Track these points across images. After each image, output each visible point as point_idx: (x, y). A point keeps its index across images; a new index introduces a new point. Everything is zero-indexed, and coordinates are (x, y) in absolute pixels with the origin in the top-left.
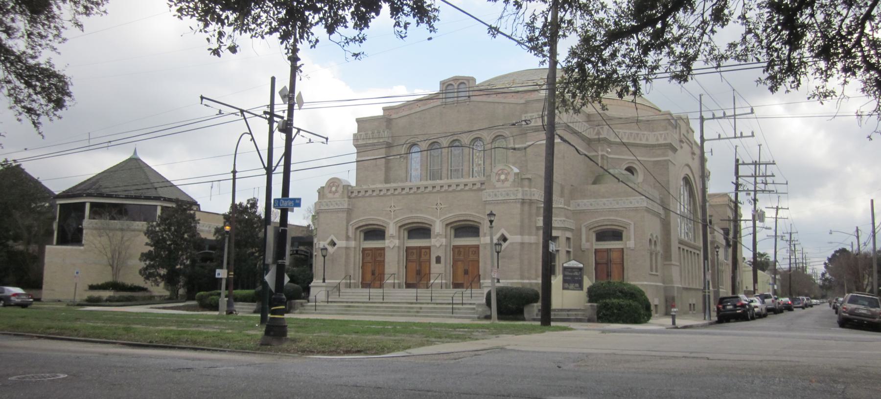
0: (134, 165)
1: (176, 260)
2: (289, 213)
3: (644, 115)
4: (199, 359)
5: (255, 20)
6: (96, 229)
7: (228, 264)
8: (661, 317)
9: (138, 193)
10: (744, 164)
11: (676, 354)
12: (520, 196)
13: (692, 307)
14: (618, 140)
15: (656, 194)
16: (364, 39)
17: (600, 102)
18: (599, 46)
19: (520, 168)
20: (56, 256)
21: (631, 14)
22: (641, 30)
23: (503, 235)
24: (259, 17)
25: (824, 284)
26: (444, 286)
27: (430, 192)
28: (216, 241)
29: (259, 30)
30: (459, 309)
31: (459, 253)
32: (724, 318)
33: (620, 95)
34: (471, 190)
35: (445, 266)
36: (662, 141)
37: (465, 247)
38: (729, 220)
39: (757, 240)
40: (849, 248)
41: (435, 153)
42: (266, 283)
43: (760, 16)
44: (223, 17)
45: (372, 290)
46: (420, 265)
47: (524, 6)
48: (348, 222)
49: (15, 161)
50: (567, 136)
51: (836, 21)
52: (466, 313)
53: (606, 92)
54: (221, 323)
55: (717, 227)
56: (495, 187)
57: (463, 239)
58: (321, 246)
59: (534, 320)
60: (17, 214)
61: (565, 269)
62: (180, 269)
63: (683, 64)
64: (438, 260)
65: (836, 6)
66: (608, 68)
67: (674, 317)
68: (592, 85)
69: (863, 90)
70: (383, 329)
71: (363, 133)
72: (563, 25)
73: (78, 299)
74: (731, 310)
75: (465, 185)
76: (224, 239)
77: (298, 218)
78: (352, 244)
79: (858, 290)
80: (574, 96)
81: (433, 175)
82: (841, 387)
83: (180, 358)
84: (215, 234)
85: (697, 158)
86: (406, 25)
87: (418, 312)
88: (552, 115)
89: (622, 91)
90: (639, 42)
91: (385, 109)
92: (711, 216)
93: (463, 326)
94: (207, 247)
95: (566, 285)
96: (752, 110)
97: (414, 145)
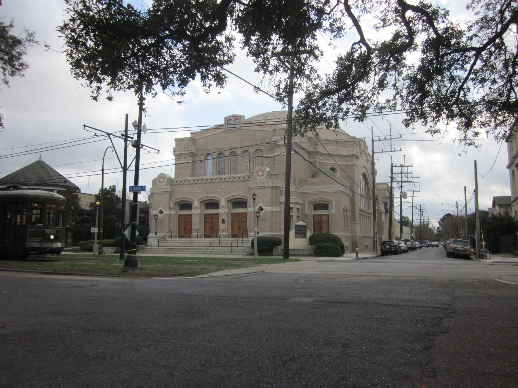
2: (139, 195)
3: (340, 138)
4: (87, 281)
7: (99, 223)
8: (349, 253)
10: (395, 166)
11: (360, 274)
12: (270, 184)
13: (367, 247)
14: (326, 152)
15: (347, 183)
16: (184, 93)
17: (315, 131)
18: (316, 99)
21: (335, 82)
24: (122, 79)
25: (438, 234)
26: (226, 236)
27: (219, 182)
30: (235, 249)
31: (235, 217)
32: (385, 253)
33: (327, 127)
34: (242, 181)
35: (227, 225)
36: (350, 153)
37: (238, 214)
38: (388, 198)
39: (403, 209)
40: (452, 213)
41: (221, 159)
45: (184, 239)
48: (170, 200)
50: (298, 150)
52: (239, 252)
53: (319, 125)
55: (380, 200)
57: (238, 209)
58: (154, 214)
59: (279, 255)
61: (296, 226)
62: (69, 228)
64: (223, 221)
67: (357, 253)
68: (312, 121)
69: (458, 128)
70: (192, 261)
71: (179, 147)
72: (296, 86)
74: (388, 249)
75: (239, 178)
76: (96, 210)
77: (142, 197)
78: (173, 212)
79: (457, 236)
80: (301, 127)
82: (451, 290)
83: (74, 280)
84: (90, 207)
85: (370, 163)
86: (210, 86)
87: (212, 252)
89: (328, 125)
91: (191, 133)
92: (377, 196)
93: (239, 260)
94: (85, 214)
95: (297, 235)
96: (400, 135)
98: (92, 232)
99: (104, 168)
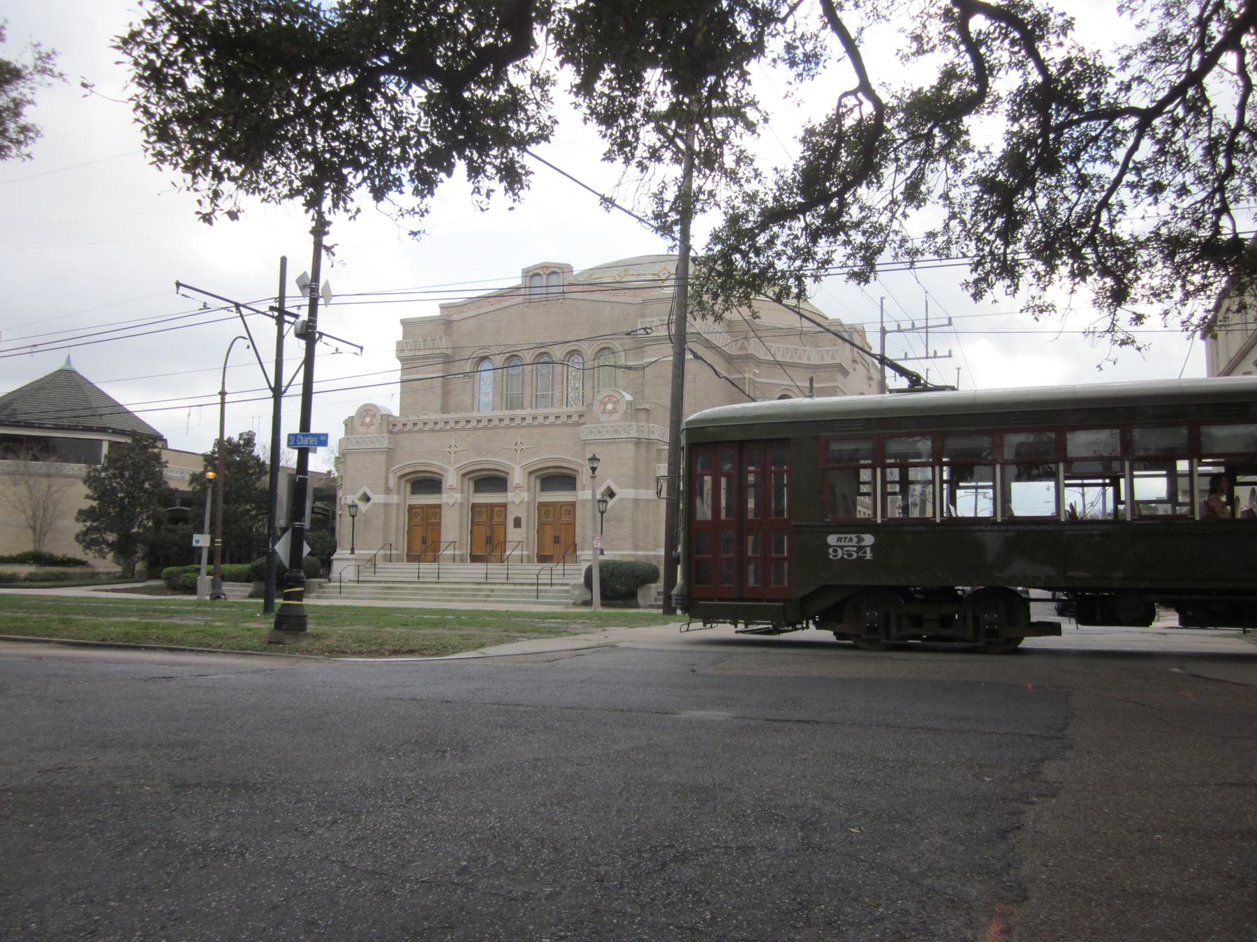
1: (131, 520)
4: (181, 664)
5: (268, 176)
6: (7, 474)
7: (212, 524)
9: (74, 422)
12: (634, 434)
14: (770, 358)
16: (427, 211)
17: (750, 307)
18: (752, 230)
19: (634, 394)
22: (809, 210)
23: (609, 488)
26: (525, 559)
28: (193, 492)
29: (274, 191)
30: (546, 591)
31: (547, 513)
34: (565, 424)
36: (828, 361)
37: (554, 504)
43: (966, 195)
44: (222, 170)
45: (422, 565)
46: (492, 528)
47: (651, 170)
48: (388, 469)
50: (701, 351)
51: (1062, 210)
52: (556, 598)
54: (205, 613)
56: (598, 421)
58: (349, 502)
59: (651, 606)
62: (138, 534)
63: (863, 258)
64: (517, 523)
65: (1063, 188)
66: (763, 260)
69: (1095, 302)
72: (701, 197)
75: (557, 417)
76: (204, 490)
77: (320, 462)
78: (394, 499)
81: (512, 403)
84: (191, 482)
87: (488, 596)
88: (682, 321)
89: (781, 292)
90: (807, 226)
91: (442, 307)
94: (178, 501)
96: (950, 319)
97: (483, 359)
98: (194, 544)
99: (227, 390)
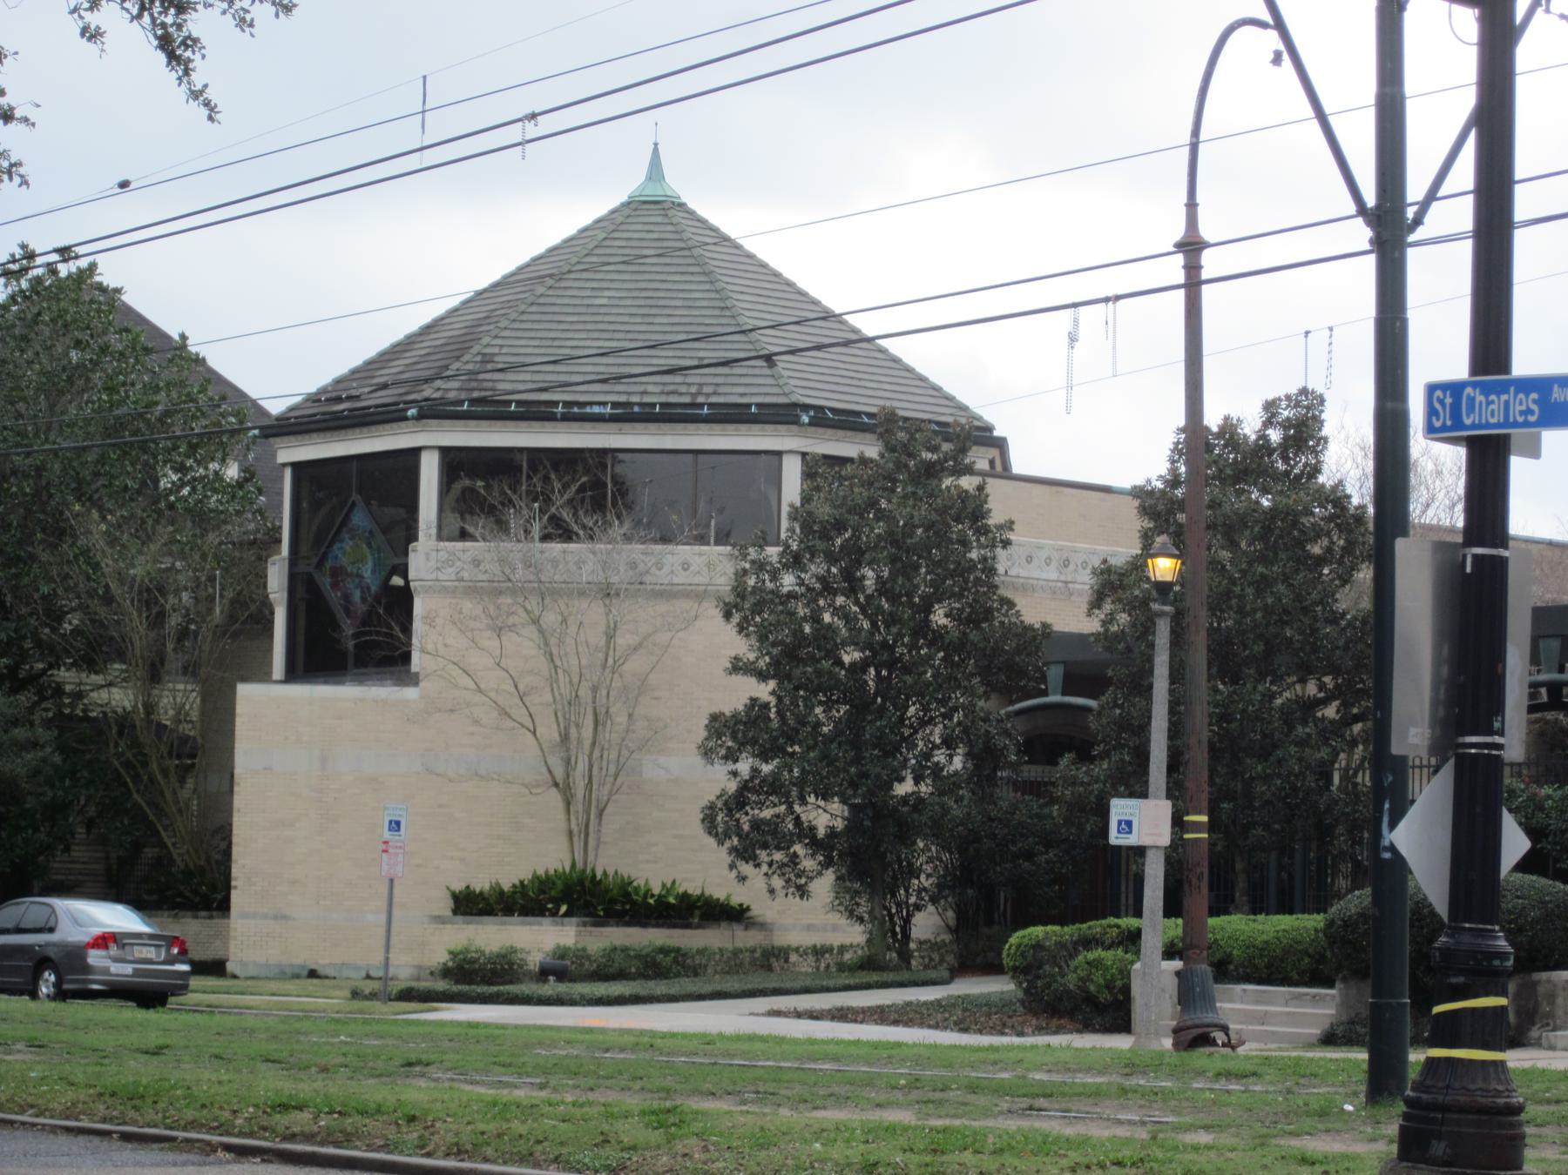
0: (654, 238)
1: (891, 747)
2: (1519, 468)
7: (1175, 763)
9: (682, 390)
20: (290, 743)
42: (1399, 862)
49: (65, 252)
60: (95, 530)
62: (916, 803)
73: (404, 969)
76: (1145, 629)
84: (1096, 603)
94: (1055, 674)
98: (1115, 838)
99: (1206, 232)
